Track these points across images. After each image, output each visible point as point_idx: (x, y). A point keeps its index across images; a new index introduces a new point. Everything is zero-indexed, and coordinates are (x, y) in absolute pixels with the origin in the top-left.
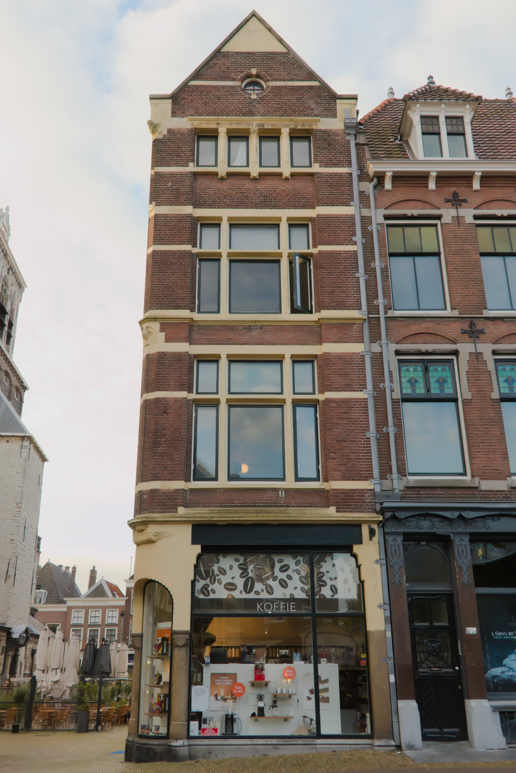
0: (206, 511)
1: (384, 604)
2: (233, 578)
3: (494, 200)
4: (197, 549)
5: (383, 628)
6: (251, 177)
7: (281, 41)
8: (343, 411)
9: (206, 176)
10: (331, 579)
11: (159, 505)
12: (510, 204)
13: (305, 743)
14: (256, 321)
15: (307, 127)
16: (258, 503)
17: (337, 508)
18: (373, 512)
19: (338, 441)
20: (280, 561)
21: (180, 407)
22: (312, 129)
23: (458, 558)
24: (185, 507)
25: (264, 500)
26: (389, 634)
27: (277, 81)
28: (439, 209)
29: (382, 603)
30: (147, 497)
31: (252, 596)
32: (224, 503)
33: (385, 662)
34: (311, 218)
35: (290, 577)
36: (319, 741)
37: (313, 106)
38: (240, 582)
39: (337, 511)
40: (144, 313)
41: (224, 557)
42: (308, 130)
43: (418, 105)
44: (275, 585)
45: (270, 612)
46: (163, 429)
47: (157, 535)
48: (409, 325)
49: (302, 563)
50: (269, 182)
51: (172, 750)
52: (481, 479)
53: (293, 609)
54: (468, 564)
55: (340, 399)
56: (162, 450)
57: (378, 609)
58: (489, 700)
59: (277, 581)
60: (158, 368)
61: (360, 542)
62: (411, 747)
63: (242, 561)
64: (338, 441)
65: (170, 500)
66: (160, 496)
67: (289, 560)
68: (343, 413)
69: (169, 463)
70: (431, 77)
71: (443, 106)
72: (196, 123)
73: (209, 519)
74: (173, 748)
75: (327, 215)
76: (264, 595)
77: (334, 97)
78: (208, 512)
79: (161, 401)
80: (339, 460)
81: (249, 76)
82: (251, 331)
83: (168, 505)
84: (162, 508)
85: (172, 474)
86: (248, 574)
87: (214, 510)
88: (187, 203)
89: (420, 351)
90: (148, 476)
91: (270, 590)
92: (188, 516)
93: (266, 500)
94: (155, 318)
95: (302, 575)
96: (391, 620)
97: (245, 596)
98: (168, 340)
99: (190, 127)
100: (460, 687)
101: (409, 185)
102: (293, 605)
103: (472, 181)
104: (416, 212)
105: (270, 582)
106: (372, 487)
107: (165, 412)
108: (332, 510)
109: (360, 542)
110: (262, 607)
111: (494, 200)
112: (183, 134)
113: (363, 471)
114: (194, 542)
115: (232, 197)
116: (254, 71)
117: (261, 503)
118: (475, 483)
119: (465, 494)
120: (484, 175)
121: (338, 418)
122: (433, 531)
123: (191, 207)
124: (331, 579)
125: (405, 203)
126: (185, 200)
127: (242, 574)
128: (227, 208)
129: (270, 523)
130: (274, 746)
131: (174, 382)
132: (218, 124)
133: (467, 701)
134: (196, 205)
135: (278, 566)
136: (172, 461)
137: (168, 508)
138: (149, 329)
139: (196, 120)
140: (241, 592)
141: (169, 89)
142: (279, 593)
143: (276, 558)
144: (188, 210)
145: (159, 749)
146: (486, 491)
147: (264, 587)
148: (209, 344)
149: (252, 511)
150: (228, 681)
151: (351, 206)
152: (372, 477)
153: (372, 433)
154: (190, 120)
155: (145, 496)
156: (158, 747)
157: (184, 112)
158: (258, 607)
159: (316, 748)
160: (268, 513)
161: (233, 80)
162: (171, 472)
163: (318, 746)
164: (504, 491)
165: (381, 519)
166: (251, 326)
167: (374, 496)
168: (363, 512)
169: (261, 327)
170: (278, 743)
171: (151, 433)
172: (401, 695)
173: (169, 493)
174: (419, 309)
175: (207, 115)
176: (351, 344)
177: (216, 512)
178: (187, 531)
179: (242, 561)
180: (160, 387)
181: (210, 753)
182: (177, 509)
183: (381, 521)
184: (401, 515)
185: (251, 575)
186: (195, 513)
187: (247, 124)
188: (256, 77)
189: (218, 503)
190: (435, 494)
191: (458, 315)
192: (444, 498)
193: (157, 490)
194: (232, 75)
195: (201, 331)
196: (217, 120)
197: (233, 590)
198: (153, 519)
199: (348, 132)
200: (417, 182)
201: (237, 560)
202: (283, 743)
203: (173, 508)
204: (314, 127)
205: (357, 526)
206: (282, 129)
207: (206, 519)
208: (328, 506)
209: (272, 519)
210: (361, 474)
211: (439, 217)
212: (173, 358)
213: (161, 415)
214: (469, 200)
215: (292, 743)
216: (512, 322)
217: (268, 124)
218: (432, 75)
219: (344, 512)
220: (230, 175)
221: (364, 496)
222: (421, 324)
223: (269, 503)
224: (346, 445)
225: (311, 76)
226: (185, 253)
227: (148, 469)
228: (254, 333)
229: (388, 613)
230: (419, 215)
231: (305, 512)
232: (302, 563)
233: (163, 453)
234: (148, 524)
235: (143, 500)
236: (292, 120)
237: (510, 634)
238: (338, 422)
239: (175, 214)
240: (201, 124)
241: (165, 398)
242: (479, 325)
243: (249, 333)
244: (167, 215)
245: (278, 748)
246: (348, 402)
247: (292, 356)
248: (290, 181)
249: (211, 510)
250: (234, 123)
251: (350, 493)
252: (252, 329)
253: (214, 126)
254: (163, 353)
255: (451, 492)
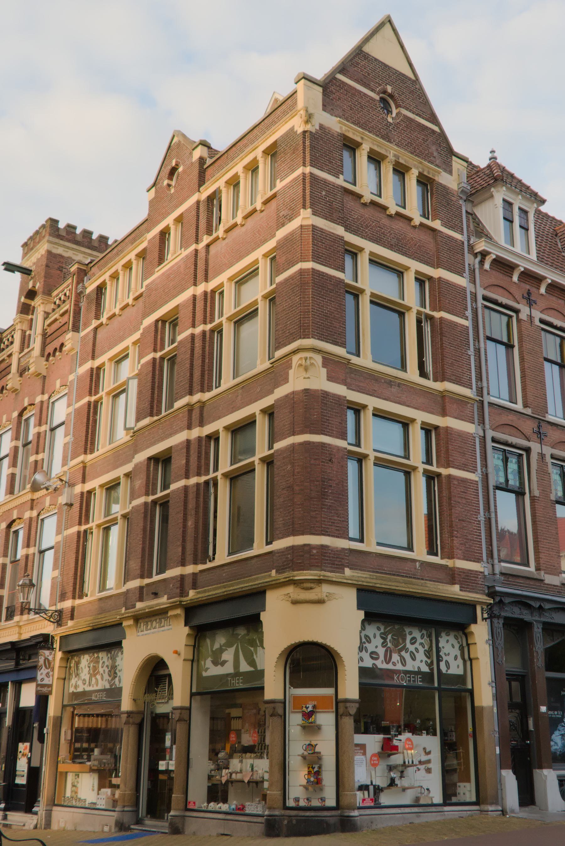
0: (364, 576)
1: (492, 682)
2: (376, 647)
3: (560, 312)
4: (361, 615)
5: (491, 705)
6: (388, 213)
7: (411, 65)
8: (463, 490)
9: (351, 196)
10: (445, 654)
11: (329, 563)
12: (506, 292)
13: (438, 810)
14: (396, 377)
15: (431, 176)
16: (401, 573)
17: (460, 587)
18: (481, 594)
19: (459, 520)
20: (411, 633)
21: (342, 458)
22: (434, 180)
23: (536, 644)
24: (351, 569)
25: (406, 570)
26: (495, 709)
27: (407, 110)
28: (519, 303)
29: (491, 681)
30: (317, 552)
31: (390, 666)
32: (376, 569)
33: (493, 735)
34: (432, 277)
35: (417, 650)
36: (446, 808)
37: (435, 154)
38: (381, 651)
39: (461, 590)
40: (429, 379)
41: (369, 624)
42: (431, 178)
43: (504, 188)
44: (407, 656)
45: (405, 684)
46: (329, 480)
47: (329, 595)
48: (500, 414)
49: (425, 637)
50: (401, 224)
51: (351, 821)
52: (545, 573)
53: (420, 681)
54: (542, 649)
55: (460, 477)
56: (329, 502)
57: (488, 686)
58: (554, 770)
59: (409, 653)
60: (322, 409)
61: (475, 622)
62: (513, 811)
63: (382, 631)
64: (459, 520)
65: (338, 560)
66: (330, 553)
67: (417, 634)
68: (462, 492)
69: (336, 518)
70: (493, 152)
71: (520, 197)
72: (344, 128)
73: (373, 585)
74: (352, 818)
75: (447, 280)
76: (399, 667)
77: (451, 152)
78: (369, 576)
79: (326, 447)
80: (461, 539)
81: (385, 92)
82: (391, 387)
83: (337, 565)
84: (331, 567)
85: (338, 530)
86: (387, 644)
87: (373, 576)
88: (339, 222)
89: (507, 442)
90: (317, 529)
91: (403, 661)
92: (354, 578)
93: (408, 570)
94: (320, 351)
95: (426, 649)
96: (497, 697)
97: (385, 666)
98: (330, 378)
99: (339, 131)
100: (529, 759)
101: (499, 270)
102: (420, 678)
103: (540, 284)
104: (505, 301)
105: (403, 653)
106: (482, 570)
107: (330, 461)
108: (456, 588)
109: (475, 622)
110: (398, 678)
111: (560, 312)
112: (332, 136)
113: (477, 553)
114: (359, 607)
115: (372, 229)
116: (389, 89)
117: (404, 573)
118: (540, 576)
119: (536, 585)
120: (498, 259)
121: (459, 497)
122: (521, 617)
123: (343, 228)
124: (445, 654)
125: (496, 288)
126: (338, 219)
127: (383, 643)
128: (369, 240)
129: (467, 602)
130: (417, 814)
131: (336, 428)
132: (362, 138)
133: (534, 770)
134: (348, 228)
135: (409, 638)
136: (338, 517)
137: (337, 568)
138: (312, 361)
139: (345, 125)
140: (382, 663)
141: (319, 74)
142: (411, 666)
143: (407, 630)
144: (339, 230)
145: (332, 821)
146: (548, 584)
147: (399, 658)
148: (358, 391)
149: (401, 581)
150: (360, 751)
151: (463, 277)
152: (482, 560)
153: (482, 517)
154: (340, 122)
155: (315, 551)
156: (331, 818)
157: (332, 109)
158: (395, 678)
159: (445, 815)
160: (413, 584)
161: (372, 90)
162: (338, 528)
163: (446, 813)
164: (557, 586)
165: (492, 602)
166: (391, 381)
167: (484, 579)
168: (477, 593)
169: (399, 385)
170: (418, 811)
171: (317, 481)
172: (503, 766)
173: (337, 551)
174: (499, 398)
175: (352, 123)
176: (466, 423)
177: (375, 577)
178: (351, 596)
179: (382, 631)
180: (324, 431)
181: (372, 823)
182: (344, 570)
183: (491, 604)
184: (547, 606)
185: (389, 645)
186: (358, 577)
187: (386, 150)
188: (388, 96)
189: (371, 568)
190: (518, 583)
191: (530, 414)
192: (523, 586)
193: (327, 547)
194: (372, 84)
195: (353, 375)
196: (363, 134)
197: (377, 659)
198: (330, 579)
199: (461, 196)
200: (506, 270)
201: (379, 629)
202: (422, 811)
203: (340, 568)
204: (436, 178)
205: (471, 606)
206: (413, 169)
207: (371, 585)
208: (454, 584)
209: (420, 591)
210: (475, 556)
211: (517, 311)
212: (335, 400)
213: (327, 463)
214: (538, 301)
215: (429, 811)
216: (563, 430)
217: (402, 159)
218: (494, 149)
219: (469, 592)
220: (373, 203)
221: (477, 578)
222: (507, 416)
223: (409, 574)
224: (465, 525)
225: (433, 119)
226: (340, 282)
227: (317, 521)
228: (394, 390)
229: (494, 692)
230: (560, 327)
231: (439, 587)
232: (425, 637)
233: (330, 506)
234: (321, 583)
235: (313, 555)
236: (421, 163)
237: (556, 713)
238: (459, 501)
239: (329, 232)
240: (349, 131)
241: (329, 445)
242: (545, 429)
243: (390, 389)
244: (323, 229)
245: (420, 816)
246: (465, 482)
247: (375, 409)
248: (417, 230)
249: (370, 575)
250: (376, 144)
251: (468, 573)
252: (392, 385)
253: (358, 139)
254: (326, 392)
255: (528, 582)
